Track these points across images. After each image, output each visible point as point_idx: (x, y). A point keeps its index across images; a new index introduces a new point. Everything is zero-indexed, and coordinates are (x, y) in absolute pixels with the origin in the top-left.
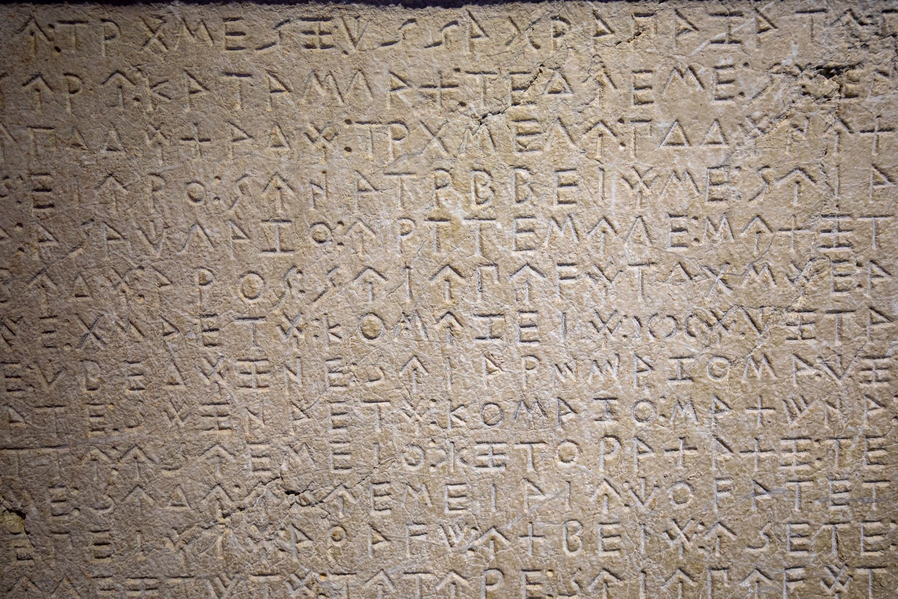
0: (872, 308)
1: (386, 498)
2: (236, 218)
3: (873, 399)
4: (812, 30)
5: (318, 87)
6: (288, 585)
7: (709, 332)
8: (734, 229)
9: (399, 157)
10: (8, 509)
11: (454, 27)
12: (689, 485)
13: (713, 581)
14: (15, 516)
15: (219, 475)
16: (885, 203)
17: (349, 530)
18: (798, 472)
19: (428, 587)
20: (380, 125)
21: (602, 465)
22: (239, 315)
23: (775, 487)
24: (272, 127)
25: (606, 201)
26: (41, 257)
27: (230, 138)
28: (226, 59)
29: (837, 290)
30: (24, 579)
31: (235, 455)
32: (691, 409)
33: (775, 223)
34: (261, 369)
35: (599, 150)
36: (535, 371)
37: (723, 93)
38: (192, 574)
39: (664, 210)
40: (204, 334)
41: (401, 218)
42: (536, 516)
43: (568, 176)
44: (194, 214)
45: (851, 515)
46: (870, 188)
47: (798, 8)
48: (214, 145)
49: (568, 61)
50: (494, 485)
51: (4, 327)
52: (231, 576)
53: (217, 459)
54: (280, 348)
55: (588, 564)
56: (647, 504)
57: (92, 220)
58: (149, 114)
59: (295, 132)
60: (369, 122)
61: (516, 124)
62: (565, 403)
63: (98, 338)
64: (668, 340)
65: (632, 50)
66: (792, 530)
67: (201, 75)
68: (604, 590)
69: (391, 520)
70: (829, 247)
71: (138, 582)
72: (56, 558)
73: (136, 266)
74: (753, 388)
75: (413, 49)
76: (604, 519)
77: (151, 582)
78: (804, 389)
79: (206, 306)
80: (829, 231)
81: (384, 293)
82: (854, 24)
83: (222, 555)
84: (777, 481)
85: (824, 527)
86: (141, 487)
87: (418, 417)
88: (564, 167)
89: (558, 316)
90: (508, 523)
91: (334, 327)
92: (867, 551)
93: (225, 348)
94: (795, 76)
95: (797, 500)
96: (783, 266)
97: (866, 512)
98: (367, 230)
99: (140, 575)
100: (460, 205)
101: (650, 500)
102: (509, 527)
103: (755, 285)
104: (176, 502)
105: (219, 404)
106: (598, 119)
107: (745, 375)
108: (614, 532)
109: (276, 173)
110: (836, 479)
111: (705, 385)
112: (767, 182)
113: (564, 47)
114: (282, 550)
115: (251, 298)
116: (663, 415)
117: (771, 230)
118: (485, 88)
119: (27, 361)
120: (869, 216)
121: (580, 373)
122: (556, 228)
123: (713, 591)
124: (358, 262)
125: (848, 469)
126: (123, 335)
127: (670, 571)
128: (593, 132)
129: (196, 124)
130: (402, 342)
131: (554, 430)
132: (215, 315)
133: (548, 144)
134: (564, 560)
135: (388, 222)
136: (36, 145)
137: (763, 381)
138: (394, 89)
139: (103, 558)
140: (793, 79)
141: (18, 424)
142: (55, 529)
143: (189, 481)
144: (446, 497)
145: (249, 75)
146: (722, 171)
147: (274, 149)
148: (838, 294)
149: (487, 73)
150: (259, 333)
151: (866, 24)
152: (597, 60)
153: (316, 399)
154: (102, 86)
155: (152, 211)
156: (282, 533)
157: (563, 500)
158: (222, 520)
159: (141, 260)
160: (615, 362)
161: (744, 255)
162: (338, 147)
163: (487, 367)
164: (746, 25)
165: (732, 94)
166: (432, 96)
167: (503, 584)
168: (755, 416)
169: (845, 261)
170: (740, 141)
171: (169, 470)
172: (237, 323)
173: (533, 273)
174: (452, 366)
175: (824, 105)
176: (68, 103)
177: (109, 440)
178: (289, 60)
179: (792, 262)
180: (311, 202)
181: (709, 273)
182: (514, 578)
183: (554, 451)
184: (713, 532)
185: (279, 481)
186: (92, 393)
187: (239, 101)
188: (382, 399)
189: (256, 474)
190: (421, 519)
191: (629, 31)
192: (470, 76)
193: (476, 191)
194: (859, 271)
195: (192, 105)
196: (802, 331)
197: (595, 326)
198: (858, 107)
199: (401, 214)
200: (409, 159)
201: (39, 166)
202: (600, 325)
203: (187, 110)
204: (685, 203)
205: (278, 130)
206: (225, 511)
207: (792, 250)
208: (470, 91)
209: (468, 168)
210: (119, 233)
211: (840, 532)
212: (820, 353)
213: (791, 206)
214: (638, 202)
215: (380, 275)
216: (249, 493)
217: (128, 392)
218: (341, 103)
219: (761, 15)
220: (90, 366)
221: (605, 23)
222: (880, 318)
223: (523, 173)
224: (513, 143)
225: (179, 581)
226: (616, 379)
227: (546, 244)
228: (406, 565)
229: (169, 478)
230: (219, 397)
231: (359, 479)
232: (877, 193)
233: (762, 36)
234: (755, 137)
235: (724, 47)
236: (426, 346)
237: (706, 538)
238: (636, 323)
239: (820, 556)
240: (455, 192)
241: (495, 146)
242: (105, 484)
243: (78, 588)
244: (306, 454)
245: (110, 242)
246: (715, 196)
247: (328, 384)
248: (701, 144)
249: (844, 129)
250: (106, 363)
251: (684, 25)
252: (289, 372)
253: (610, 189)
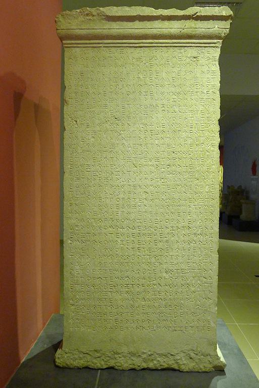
28: (108, 55)
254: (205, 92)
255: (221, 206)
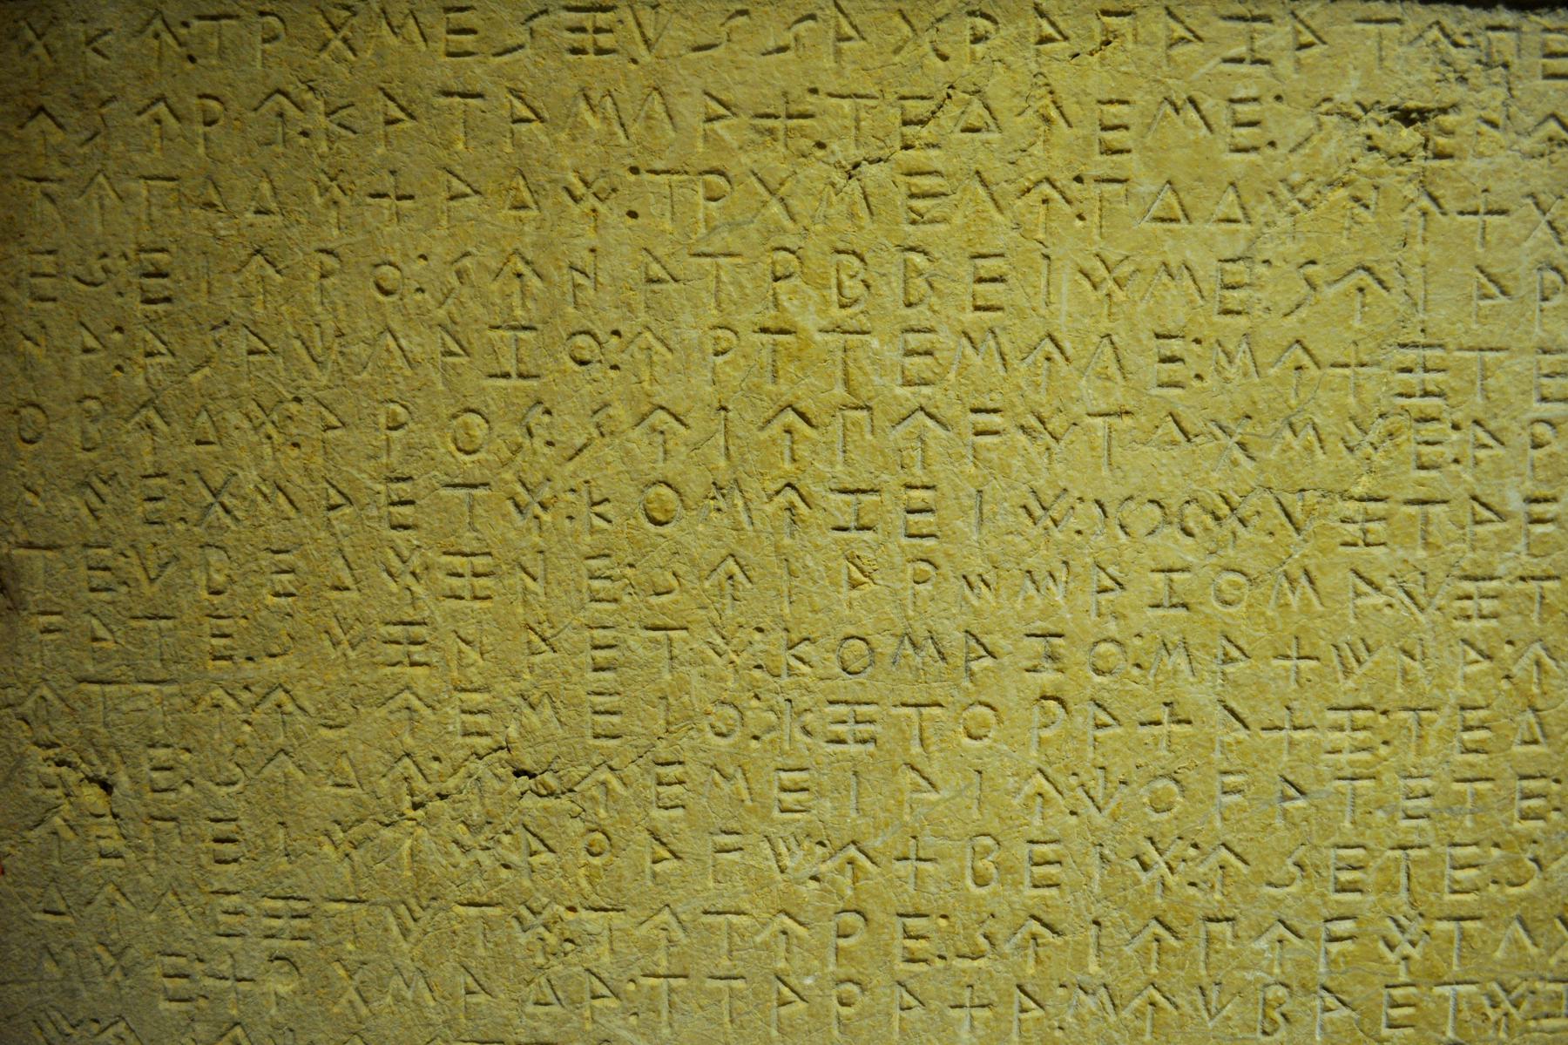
0: (1475, 498)
1: (677, 789)
2: (448, 322)
3: (1472, 646)
4: (1380, 49)
5: (588, 116)
6: (514, 923)
7: (1216, 529)
8: (1259, 361)
9: (715, 228)
10: (87, 777)
11: (810, 23)
12: (1177, 782)
13: (1209, 940)
14: (97, 789)
15: (408, 740)
16: (1496, 329)
17: (615, 838)
18: (1351, 764)
19: (742, 936)
20: (685, 177)
21: (1034, 746)
22: (447, 479)
23: (1315, 788)
24: (512, 178)
25: (1052, 308)
26: (147, 380)
27: (445, 195)
28: (444, 71)
29: (1422, 467)
30: (109, 888)
31: (434, 709)
32: (1184, 656)
33: (1325, 353)
34: (480, 570)
35: (1041, 226)
36: (928, 586)
37: (1243, 142)
38: (364, 896)
39: (1146, 327)
40: (392, 509)
41: (714, 328)
42: (922, 828)
43: (990, 266)
44: (383, 315)
45: (1432, 833)
46: (1473, 304)
47: (1359, 15)
48: (419, 205)
49: (993, 81)
50: (855, 773)
51: (89, 491)
52: (424, 903)
53: (405, 714)
54: (512, 535)
55: (1006, 906)
56: (1106, 812)
57: (227, 323)
58: (321, 157)
59: (548, 186)
60: (667, 172)
61: (907, 179)
62: (978, 641)
63: (227, 511)
64: (1150, 540)
65: (1097, 67)
66: (1339, 858)
67: (404, 95)
68: (1030, 952)
69: (683, 825)
70: (1410, 396)
71: (280, 904)
72: (156, 859)
73: (290, 397)
74: (1286, 623)
75: (744, 56)
76: (1036, 835)
77: (300, 906)
78: (1366, 627)
79: (396, 465)
80: (1410, 371)
81: (683, 449)
82: (1444, 44)
83: (411, 869)
84: (1319, 778)
85: (1390, 853)
86: (287, 754)
87: (734, 657)
88: (984, 251)
89: (970, 496)
90: (876, 836)
91: (599, 503)
92: (1454, 892)
93: (423, 533)
94: (1356, 120)
95: (1348, 809)
96: (1336, 425)
97: (1456, 829)
98: (658, 346)
99: (282, 894)
100: (812, 308)
101: (1113, 805)
102: (878, 843)
103: (1291, 454)
104: (340, 781)
105: (411, 624)
106: (1040, 176)
107: (1272, 602)
108: (1052, 857)
109: (516, 252)
110: (1411, 777)
111: (1207, 616)
112: (1313, 287)
113: (988, 59)
114: (506, 866)
115: (468, 453)
116: (1138, 666)
117: (1317, 364)
118: (857, 120)
119: (120, 544)
120: (1471, 349)
121: (1002, 591)
122: (969, 350)
123: (1207, 955)
124: (643, 397)
125: (1431, 759)
126: (266, 507)
127: (1140, 922)
128: (1034, 197)
129: (393, 173)
130: (709, 531)
131: (958, 686)
132: (410, 478)
133: (960, 214)
134: (968, 900)
135: (694, 334)
136: (150, 205)
137: (1301, 612)
138: (709, 120)
139: (226, 862)
140: (1353, 125)
141: (104, 644)
142: (156, 813)
143: (361, 747)
144: (776, 791)
145: (479, 96)
146: (1240, 266)
147: (514, 213)
148: (1423, 473)
149: (861, 97)
150: (479, 510)
151: (1462, 46)
152: (1041, 81)
153: (567, 621)
154: (253, 115)
155: (318, 309)
156: (506, 839)
157: (968, 802)
158: (411, 813)
159: (298, 388)
160: (1061, 575)
161: (1275, 405)
162: (616, 211)
163: (850, 577)
164: (1276, 37)
165: (1256, 143)
166: (771, 131)
167: (866, 936)
168: (1287, 670)
169: (1434, 419)
170: (1269, 219)
171: (331, 727)
172: (444, 492)
173: (930, 423)
174: (791, 573)
175: (1400, 169)
176: (201, 141)
177: (239, 676)
178: (544, 72)
179: (1351, 418)
180: (570, 298)
181: (1218, 432)
182: (883, 926)
183: (956, 719)
184: (1213, 861)
185: (503, 754)
186: (216, 600)
187: (462, 136)
188: (674, 624)
189: (468, 740)
190: (734, 825)
191: (1092, 38)
192: (834, 101)
193: (839, 286)
194: (1455, 436)
195: (388, 143)
196: (1365, 532)
197: (1030, 515)
198: (1452, 173)
199: (716, 321)
200: (730, 231)
201: (152, 237)
202: (1038, 512)
203: (381, 150)
204: (1182, 315)
205: (522, 182)
206: (416, 799)
207: (1351, 400)
208: (834, 124)
209: (827, 248)
210: (266, 344)
211: (1414, 861)
212: (1392, 569)
213: (1350, 328)
214: (1105, 311)
215: (678, 419)
216: (455, 772)
217: (271, 600)
218: (623, 141)
219: (1301, 22)
220: (214, 556)
221: (1053, 24)
222: (1487, 514)
223: (918, 259)
224: (902, 210)
225: (343, 906)
226: (1062, 602)
227: (951, 376)
228: (707, 899)
229: (330, 741)
230: (411, 612)
231: (634, 757)
232: (1482, 312)
233: (1303, 54)
234: (1293, 214)
235: (1244, 68)
236: (750, 539)
237: (1201, 869)
238: (1097, 511)
239: (1381, 900)
240: (804, 287)
241: (871, 213)
242: (232, 746)
243: (189, 907)
244: (548, 712)
245: (252, 358)
246: (1229, 306)
247: (586, 598)
248: (1207, 221)
249: (1432, 208)
250: (238, 551)
251: (1180, 31)
252: (524, 576)
253: (1059, 289)
254: (1515, 503)
255: (1500, 7)
